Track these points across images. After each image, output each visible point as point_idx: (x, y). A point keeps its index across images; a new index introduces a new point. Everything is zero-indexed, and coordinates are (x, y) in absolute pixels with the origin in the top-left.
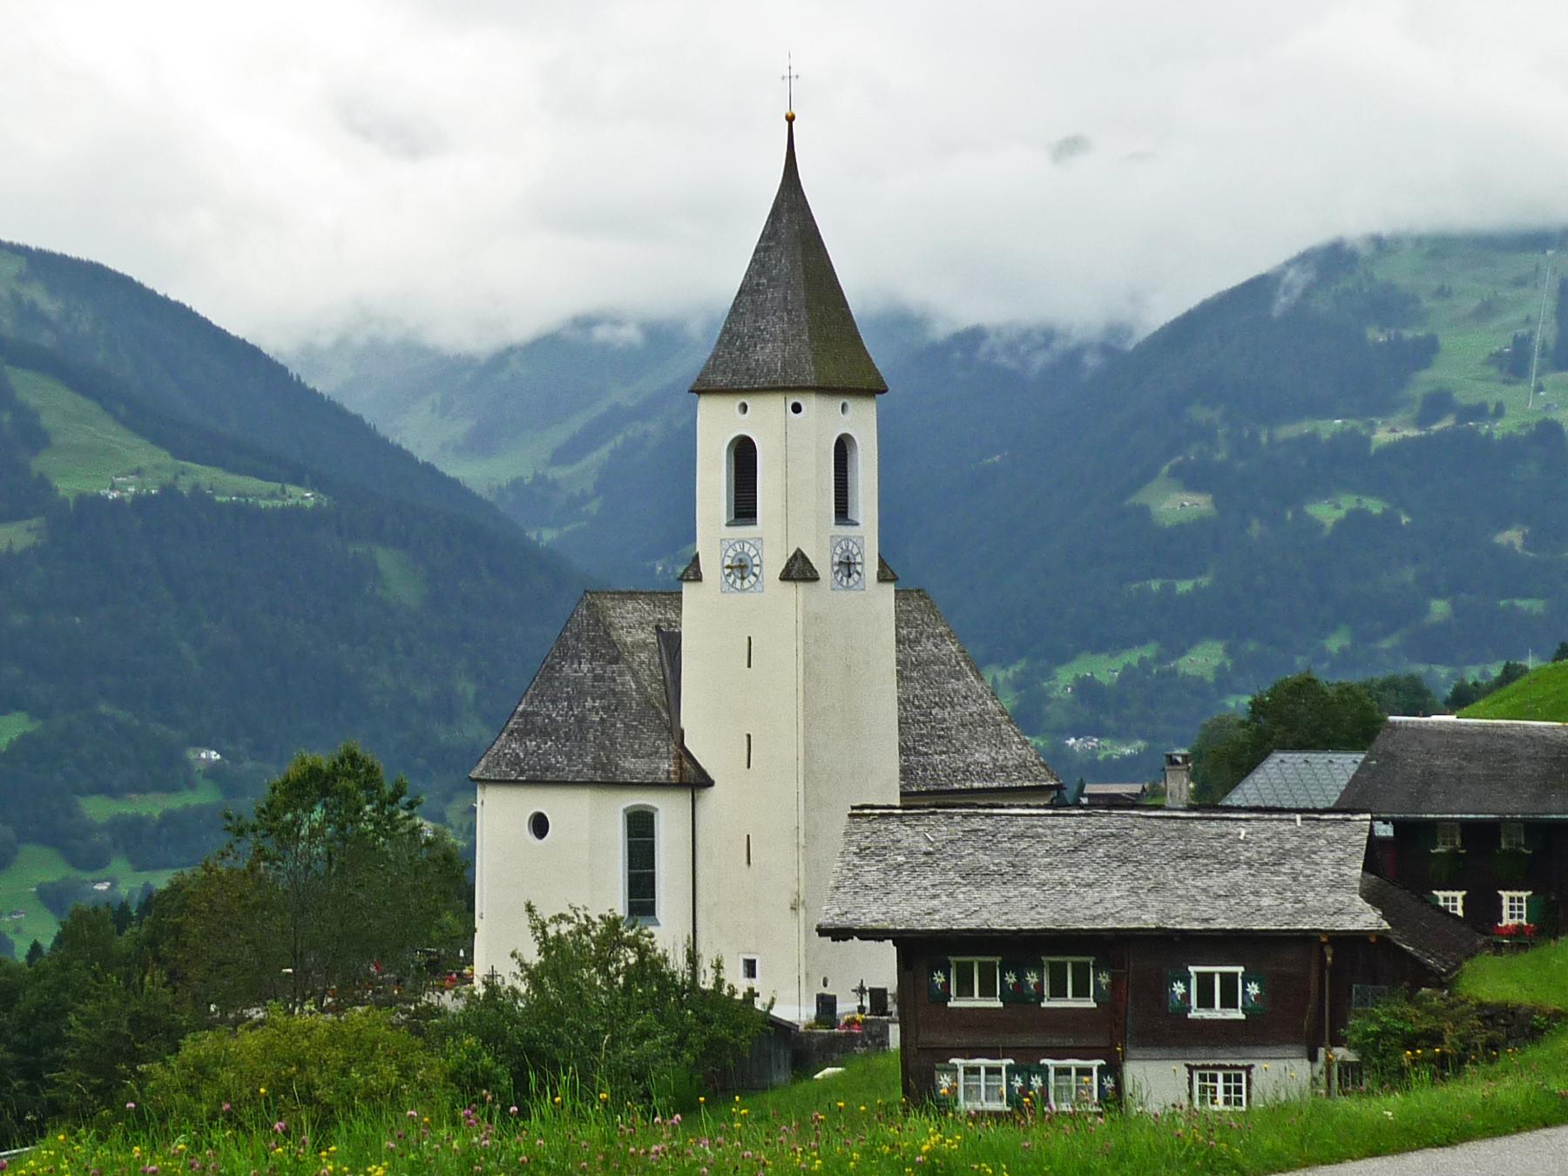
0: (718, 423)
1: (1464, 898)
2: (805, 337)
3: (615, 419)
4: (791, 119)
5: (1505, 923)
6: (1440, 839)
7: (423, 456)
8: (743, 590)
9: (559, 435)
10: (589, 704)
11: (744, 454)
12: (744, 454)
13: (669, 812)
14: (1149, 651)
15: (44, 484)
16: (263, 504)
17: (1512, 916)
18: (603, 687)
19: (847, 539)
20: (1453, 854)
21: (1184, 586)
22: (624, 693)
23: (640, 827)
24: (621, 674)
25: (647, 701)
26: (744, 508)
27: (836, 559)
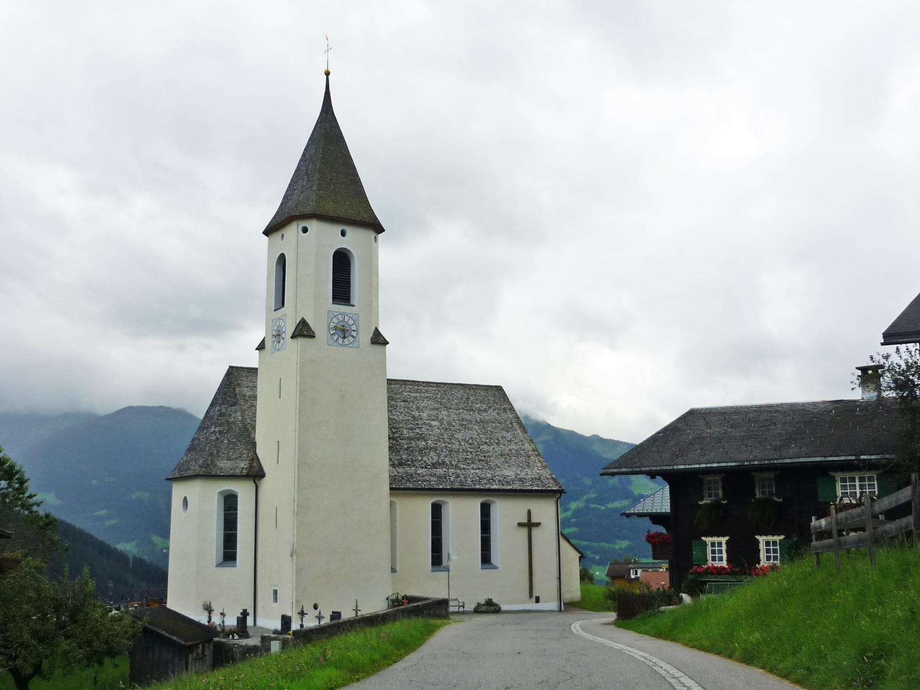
1: (759, 561)
2: (314, 188)
4: (327, 74)
5: (762, 563)
6: (706, 493)
8: (343, 345)
10: (212, 429)
13: (243, 491)
17: (768, 558)
18: (223, 420)
19: (344, 314)
20: (717, 505)
22: (234, 423)
23: (230, 502)
24: (236, 411)
25: (245, 428)
27: (332, 325)
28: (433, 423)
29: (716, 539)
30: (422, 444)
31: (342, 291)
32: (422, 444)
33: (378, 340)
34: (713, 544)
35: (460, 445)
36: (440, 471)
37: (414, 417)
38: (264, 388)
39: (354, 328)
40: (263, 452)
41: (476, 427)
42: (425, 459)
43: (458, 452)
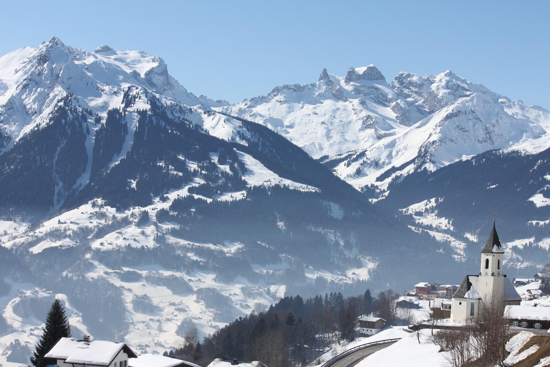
0: (484, 257)
3: (394, 169)
7: (342, 178)
9: (380, 172)
11: (487, 261)
12: (487, 261)
14: (532, 240)
15: (245, 183)
16: (302, 190)
21: (542, 223)
26: (487, 267)
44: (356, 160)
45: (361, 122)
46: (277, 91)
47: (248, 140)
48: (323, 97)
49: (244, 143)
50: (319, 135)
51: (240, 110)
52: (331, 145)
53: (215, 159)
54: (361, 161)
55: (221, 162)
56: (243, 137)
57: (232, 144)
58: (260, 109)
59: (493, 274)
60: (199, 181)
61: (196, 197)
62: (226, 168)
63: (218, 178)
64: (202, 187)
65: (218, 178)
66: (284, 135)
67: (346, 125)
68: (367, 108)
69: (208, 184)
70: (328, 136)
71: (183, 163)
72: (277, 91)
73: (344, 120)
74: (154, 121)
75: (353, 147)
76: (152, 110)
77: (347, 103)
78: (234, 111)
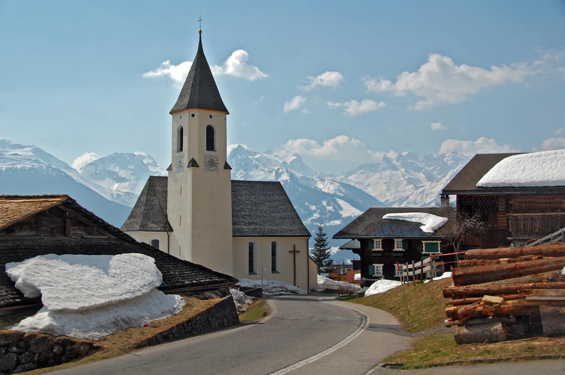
1: (395, 274)
8: (211, 171)
28: (248, 202)
29: (378, 265)
30: (243, 213)
31: (210, 145)
32: (243, 213)
33: (227, 167)
34: (377, 267)
35: (261, 213)
36: (252, 227)
37: (238, 199)
38: (171, 187)
39: (216, 162)
40: (171, 219)
41: (268, 204)
42: (245, 221)
43: (260, 217)
44: (404, 201)
45: (406, 181)
46: (360, 168)
47: (343, 193)
48: (385, 169)
49: (340, 194)
50: (384, 189)
51: (341, 179)
52: (390, 194)
53: (324, 203)
54: (407, 202)
55: (328, 205)
56: (340, 191)
57: (335, 195)
58: (351, 177)
59: (193, 163)
60: (316, 216)
61: (315, 224)
62: (330, 208)
63: (326, 213)
64: (318, 218)
65: (326, 213)
66: (365, 190)
67: (398, 183)
68: (409, 174)
69: (321, 217)
70: (388, 189)
71: (308, 206)
72: (360, 168)
73: (397, 181)
74: (292, 186)
75: (403, 194)
76: (290, 179)
77: (398, 171)
78: (338, 179)
